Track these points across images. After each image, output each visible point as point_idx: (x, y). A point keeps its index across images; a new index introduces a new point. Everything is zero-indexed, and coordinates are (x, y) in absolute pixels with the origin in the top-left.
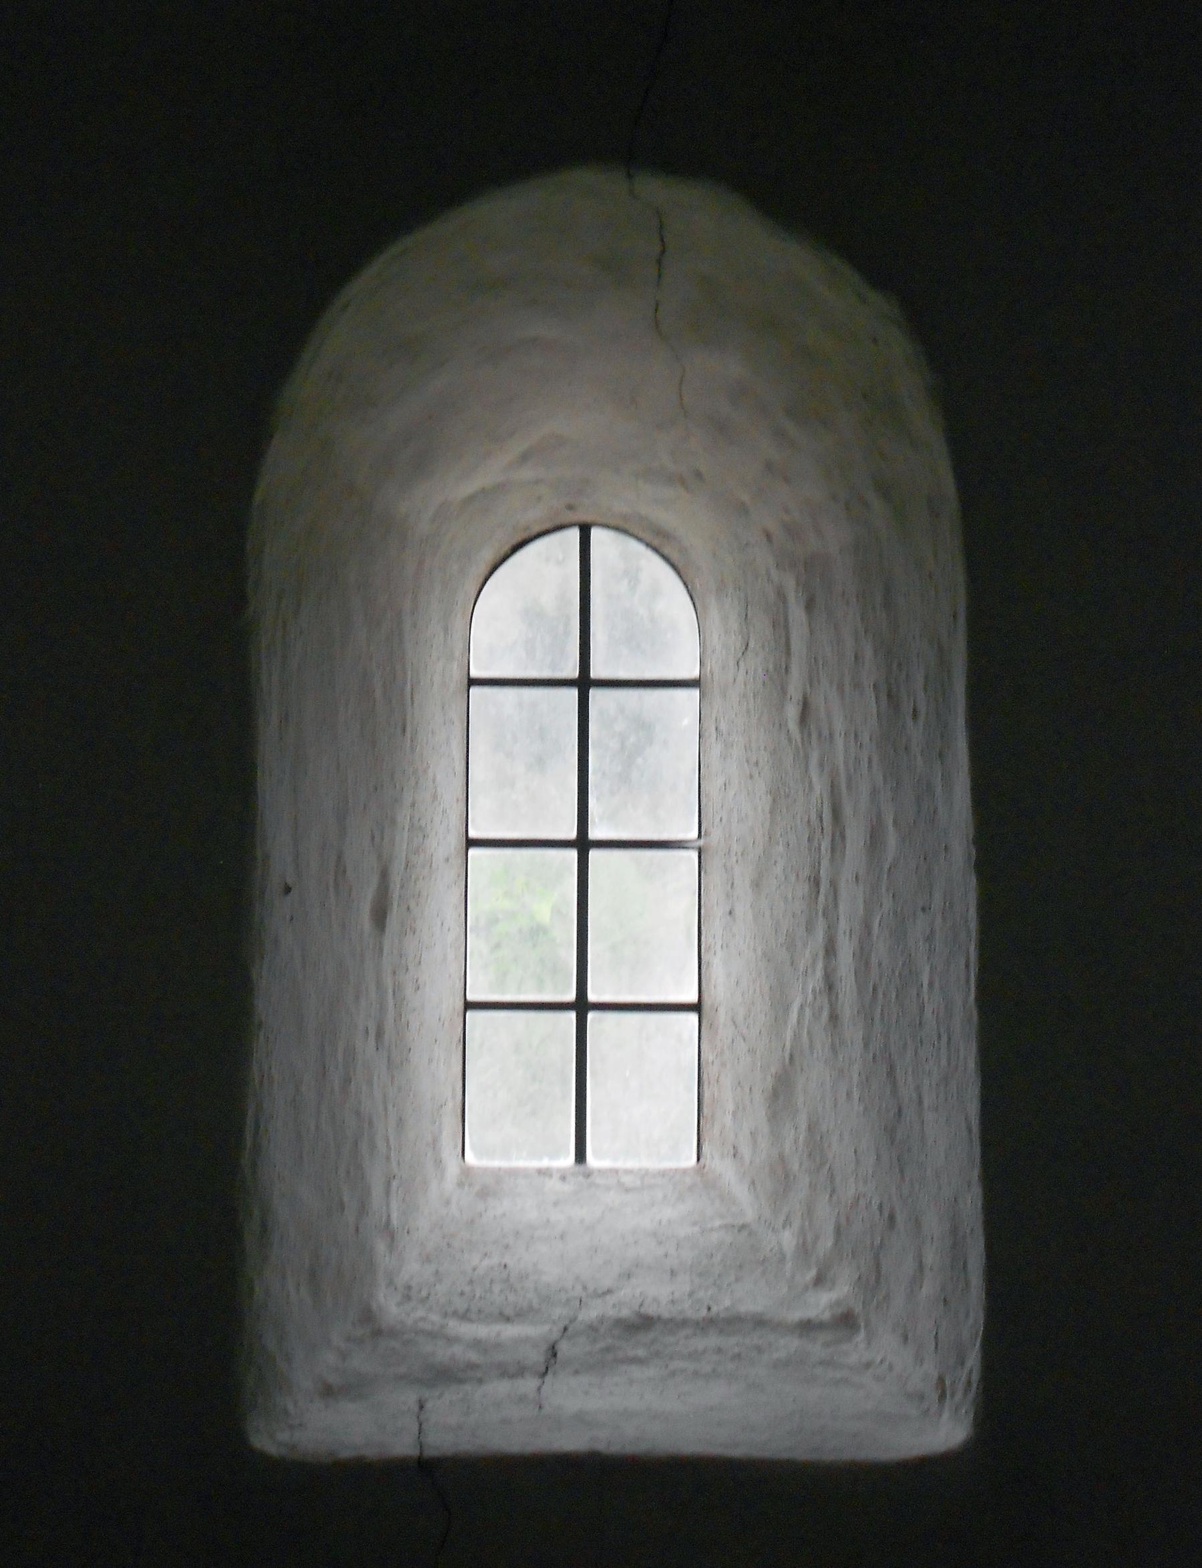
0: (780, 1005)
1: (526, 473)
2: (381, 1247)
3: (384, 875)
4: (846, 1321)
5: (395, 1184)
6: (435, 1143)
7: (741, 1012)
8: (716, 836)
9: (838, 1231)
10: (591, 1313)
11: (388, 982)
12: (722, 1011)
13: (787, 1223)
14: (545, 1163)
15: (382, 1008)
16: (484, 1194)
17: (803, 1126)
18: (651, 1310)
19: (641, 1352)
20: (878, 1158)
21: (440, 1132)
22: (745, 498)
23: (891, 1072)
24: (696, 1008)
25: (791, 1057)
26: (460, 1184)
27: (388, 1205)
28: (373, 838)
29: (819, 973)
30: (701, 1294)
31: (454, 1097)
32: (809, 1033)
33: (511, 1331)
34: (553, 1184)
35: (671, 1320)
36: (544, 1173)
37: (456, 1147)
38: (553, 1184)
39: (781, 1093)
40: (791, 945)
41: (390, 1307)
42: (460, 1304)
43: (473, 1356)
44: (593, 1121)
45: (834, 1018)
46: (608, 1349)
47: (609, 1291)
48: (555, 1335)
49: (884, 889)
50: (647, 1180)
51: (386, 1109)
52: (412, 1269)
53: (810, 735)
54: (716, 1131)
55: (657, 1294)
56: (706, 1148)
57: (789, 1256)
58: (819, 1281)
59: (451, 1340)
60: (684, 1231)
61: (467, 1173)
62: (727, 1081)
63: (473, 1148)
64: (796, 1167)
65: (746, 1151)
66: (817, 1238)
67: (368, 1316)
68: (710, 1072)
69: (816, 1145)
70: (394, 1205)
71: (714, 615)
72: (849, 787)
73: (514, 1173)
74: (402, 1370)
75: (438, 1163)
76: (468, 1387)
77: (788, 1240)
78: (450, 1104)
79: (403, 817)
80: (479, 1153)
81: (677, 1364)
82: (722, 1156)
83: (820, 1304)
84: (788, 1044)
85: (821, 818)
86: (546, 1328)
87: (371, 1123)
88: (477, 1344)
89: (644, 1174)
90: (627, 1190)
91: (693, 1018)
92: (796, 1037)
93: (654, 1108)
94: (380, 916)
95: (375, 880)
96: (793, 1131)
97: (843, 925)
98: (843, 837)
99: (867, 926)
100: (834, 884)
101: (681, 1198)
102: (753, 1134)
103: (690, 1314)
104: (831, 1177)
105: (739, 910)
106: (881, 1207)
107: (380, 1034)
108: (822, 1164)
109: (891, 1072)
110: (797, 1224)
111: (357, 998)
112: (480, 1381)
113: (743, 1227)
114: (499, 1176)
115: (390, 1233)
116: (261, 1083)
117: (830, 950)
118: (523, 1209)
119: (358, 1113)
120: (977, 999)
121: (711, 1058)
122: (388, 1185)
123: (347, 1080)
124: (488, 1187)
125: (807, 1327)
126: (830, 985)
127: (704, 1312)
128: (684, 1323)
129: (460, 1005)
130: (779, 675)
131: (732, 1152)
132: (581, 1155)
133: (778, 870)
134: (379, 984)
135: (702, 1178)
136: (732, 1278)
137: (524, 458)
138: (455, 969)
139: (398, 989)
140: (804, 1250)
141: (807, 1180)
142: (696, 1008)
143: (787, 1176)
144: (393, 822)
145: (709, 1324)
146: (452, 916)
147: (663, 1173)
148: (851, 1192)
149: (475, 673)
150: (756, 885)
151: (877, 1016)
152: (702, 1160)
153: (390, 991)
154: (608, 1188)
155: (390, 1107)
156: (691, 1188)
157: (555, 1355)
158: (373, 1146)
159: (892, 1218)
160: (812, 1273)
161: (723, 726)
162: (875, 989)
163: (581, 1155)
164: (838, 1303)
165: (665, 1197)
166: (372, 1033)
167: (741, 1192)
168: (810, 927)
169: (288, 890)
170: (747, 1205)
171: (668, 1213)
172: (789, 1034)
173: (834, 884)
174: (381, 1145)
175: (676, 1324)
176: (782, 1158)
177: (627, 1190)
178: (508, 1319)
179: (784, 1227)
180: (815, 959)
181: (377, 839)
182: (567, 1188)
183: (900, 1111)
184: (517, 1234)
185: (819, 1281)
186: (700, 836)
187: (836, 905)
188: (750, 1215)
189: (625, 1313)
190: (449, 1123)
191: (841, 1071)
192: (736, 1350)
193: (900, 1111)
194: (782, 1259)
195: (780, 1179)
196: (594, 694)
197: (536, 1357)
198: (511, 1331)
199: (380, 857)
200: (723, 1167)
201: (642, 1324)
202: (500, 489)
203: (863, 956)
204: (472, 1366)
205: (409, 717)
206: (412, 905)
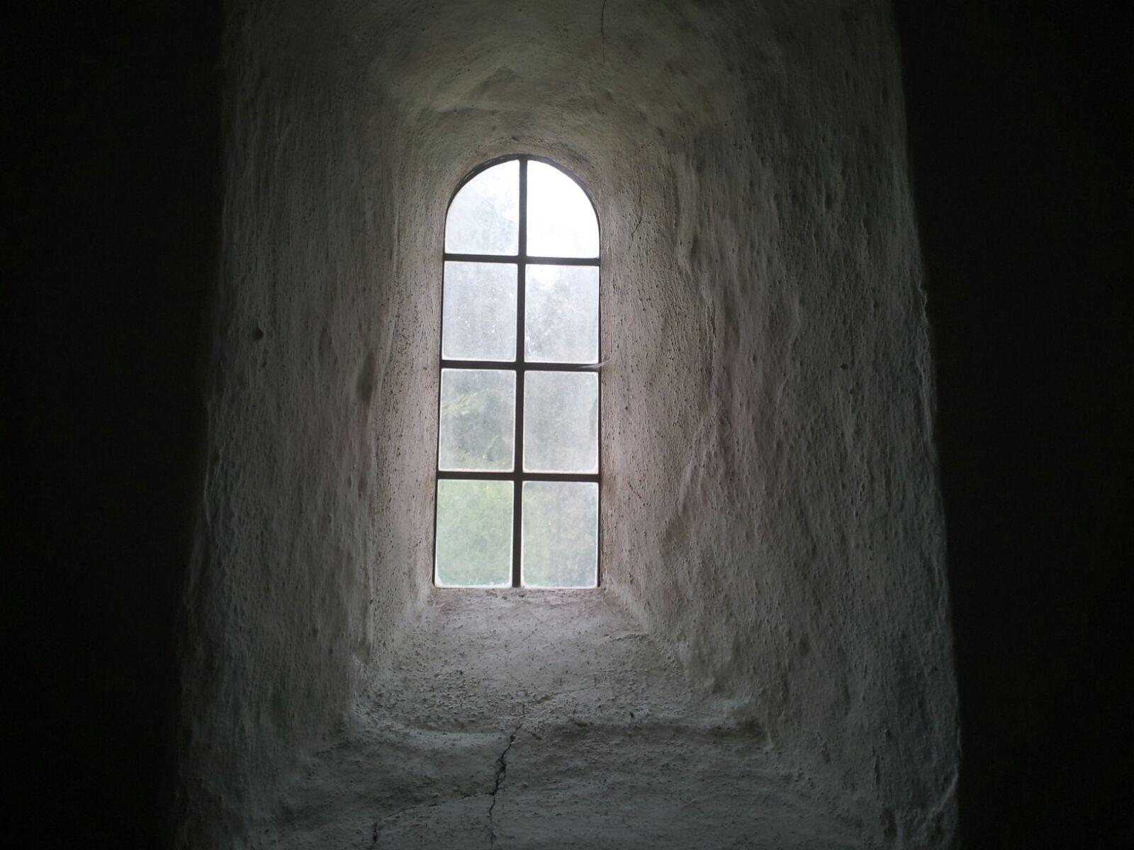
0: (673, 468)
1: (485, 104)
2: (356, 661)
3: (370, 361)
4: (751, 729)
5: (372, 607)
6: (411, 573)
7: (637, 477)
8: (614, 357)
9: (737, 649)
10: (533, 722)
11: (373, 444)
12: (619, 479)
13: (682, 636)
14: (491, 586)
15: (365, 464)
16: (447, 610)
17: (698, 561)
18: (583, 717)
19: (580, 763)
20: (787, 590)
21: (415, 564)
22: (643, 107)
23: (802, 514)
24: (596, 478)
25: (685, 508)
26: (430, 602)
27: (365, 625)
28: (360, 327)
29: (714, 439)
30: (622, 700)
31: (427, 538)
32: (702, 487)
33: (467, 740)
34: (498, 602)
35: (602, 727)
36: (491, 593)
37: (427, 575)
38: (498, 602)
39: (674, 537)
40: (683, 422)
41: (359, 712)
42: (422, 712)
43: (430, 771)
44: (525, 556)
45: (731, 474)
46: (550, 760)
47: (547, 698)
48: (504, 747)
49: (788, 360)
50: (565, 601)
51: (365, 545)
52: (385, 677)
53: (700, 264)
54: (615, 564)
55: (584, 699)
56: (606, 576)
57: (685, 664)
58: (718, 689)
59: (413, 752)
60: (600, 641)
61: (436, 592)
62: (624, 527)
63: (440, 576)
64: (690, 592)
65: (642, 580)
66: (712, 652)
67: (339, 727)
68: (610, 522)
69: (710, 576)
70: (371, 624)
71: (613, 210)
72: (743, 289)
73: (469, 593)
74: (361, 788)
75: (413, 587)
76: (422, 808)
77: (683, 650)
78: (424, 543)
79: (389, 320)
80: (446, 578)
81: (615, 777)
82: (620, 582)
83: (724, 710)
84: (681, 499)
85: (713, 321)
86: (497, 736)
87: (349, 558)
88: (435, 756)
89: (562, 594)
90: (553, 607)
91: (594, 486)
92: (690, 492)
93: (564, 544)
94: (366, 389)
95: (361, 362)
96: (686, 565)
97: (738, 398)
98: (737, 331)
99: (768, 395)
100: (727, 370)
101: (592, 614)
102: (648, 568)
103: (616, 721)
104: (728, 602)
105: (634, 404)
106: (790, 634)
107: (362, 485)
108: (718, 592)
109: (802, 514)
110: (691, 639)
111: (340, 449)
112: (434, 801)
113: (644, 637)
114: (458, 595)
115: (365, 649)
116: (215, 517)
117: (725, 419)
118: (475, 623)
119: (337, 549)
120: (936, 438)
121: (610, 512)
122: (365, 610)
123: (326, 521)
124: (450, 604)
125: (718, 734)
126: (725, 447)
127: (628, 719)
128: (614, 731)
129: (433, 473)
130: (668, 236)
131: (629, 579)
132: (516, 581)
133: (670, 370)
134: (363, 444)
135: (602, 598)
136: (644, 685)
137: (485, 86)
138: (430, 447)
139: (381, 452)
140: (701, 661)
141: (702, 604)
142: (596, 478)
143: (681, 600)
144: (380, 321)
145: (636, 732)
146: (428, 409)
147: (576, 594)
148: (752, 618)
149: (448, 251)
150: (650, 384)
151: (783, 469)
152: (603, 585)
153: (374, 451)
154: (538, 606)
155: (370, 544)
156: (598, 606)
157: (503, 769)
158: (350, 575)
159: (804, 646)
160: (709, 682)
161: (620, 283)
162: (779, 445)
163: (516, 581)
164: (741, 712)
165: (580, 612)
166: (355, 483)
167: (638, 609)
168: (703, 406)
169: (258, 335)
170: (643, 619)
171: (585, 626)
172: (682, 492)
173: (727, 370)
174: (359, 577)
175: (606, 731)
176: (675, 583)
177: (553, 607)
178: (462, 727)
179: (679, 640)
180: (708, 429)
181: (364, 327)
182: (508, 605)
183: (814, 550)
184: (471, 644)
185: (718, 689)
186: (600, 361)
187: (730, 386)
188: (647, 629)
189: (563, 720)
190: (423, 556)
191: (739, 517)
192: (665, 761)
193: (814, 550)
194: (680, 666)
195: (674, 603)
196: (530, 268)
197: (486, 771)
198: (467, 740)
199: (366, 344)
200: (624, 593)
201: (576, 732)
202: (465, 114)
203: (764, 421)
204: (429, 783)
205: (396, 248)
206: (395, 390)
